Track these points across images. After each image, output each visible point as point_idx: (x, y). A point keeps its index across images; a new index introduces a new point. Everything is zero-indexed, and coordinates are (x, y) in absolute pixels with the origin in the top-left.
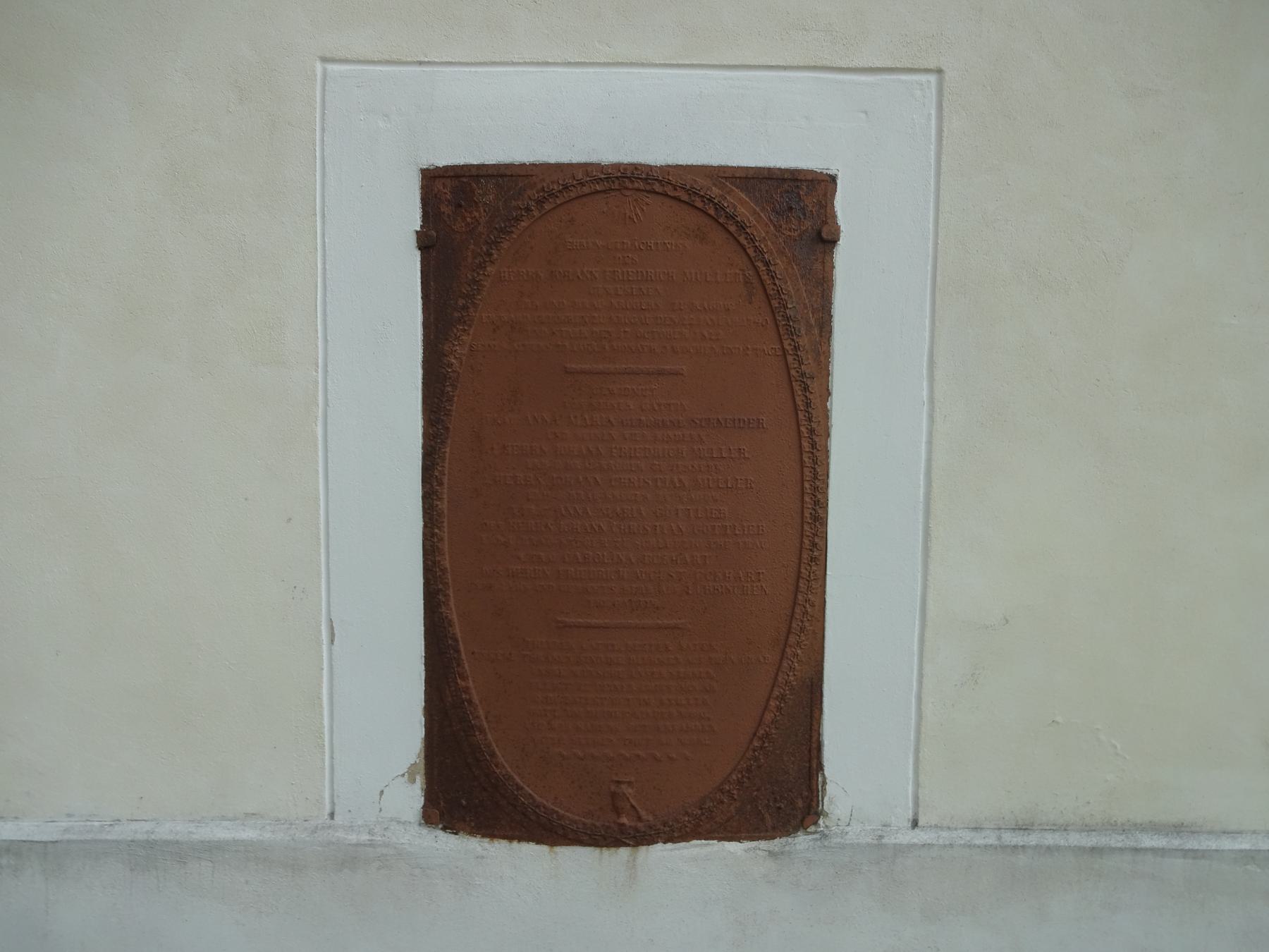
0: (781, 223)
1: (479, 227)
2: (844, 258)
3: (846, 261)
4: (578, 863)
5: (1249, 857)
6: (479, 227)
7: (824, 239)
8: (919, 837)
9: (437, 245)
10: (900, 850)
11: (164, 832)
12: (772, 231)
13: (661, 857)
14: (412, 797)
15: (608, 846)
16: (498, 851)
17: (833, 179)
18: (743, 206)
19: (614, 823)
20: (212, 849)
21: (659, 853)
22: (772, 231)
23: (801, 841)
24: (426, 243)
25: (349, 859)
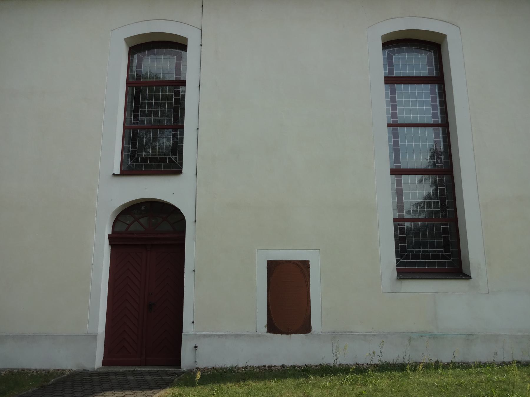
0: (305, 265)
1: (274, 267)
2: (310, 269)
3: (311, 269)
4: (284, 336)
5: (359, 335)
6: (274, 267)
7: (309, 267)
8: (290, 350)
9: (268, 268)
10: (320, 334)
11: (238, 333)
12: (303, 266)
13: (293, 335)
14: (266, 329)
15: (131, 389)
16: (275, 335)
17: (309, 261)
18: (300, 264)
19: (288, 332)
20: (245, 335)
21: (293, 335)
22: (303, 266)
23: (309, 334)
24: (267, 268)
25: (259, 336)
